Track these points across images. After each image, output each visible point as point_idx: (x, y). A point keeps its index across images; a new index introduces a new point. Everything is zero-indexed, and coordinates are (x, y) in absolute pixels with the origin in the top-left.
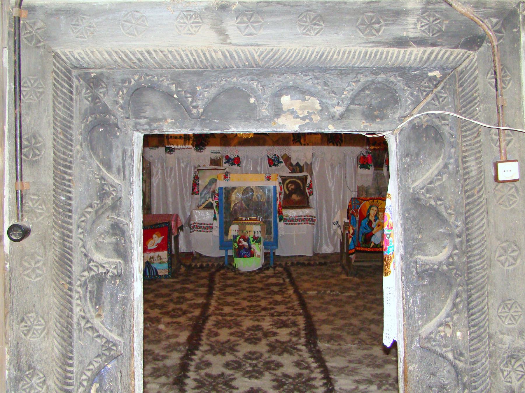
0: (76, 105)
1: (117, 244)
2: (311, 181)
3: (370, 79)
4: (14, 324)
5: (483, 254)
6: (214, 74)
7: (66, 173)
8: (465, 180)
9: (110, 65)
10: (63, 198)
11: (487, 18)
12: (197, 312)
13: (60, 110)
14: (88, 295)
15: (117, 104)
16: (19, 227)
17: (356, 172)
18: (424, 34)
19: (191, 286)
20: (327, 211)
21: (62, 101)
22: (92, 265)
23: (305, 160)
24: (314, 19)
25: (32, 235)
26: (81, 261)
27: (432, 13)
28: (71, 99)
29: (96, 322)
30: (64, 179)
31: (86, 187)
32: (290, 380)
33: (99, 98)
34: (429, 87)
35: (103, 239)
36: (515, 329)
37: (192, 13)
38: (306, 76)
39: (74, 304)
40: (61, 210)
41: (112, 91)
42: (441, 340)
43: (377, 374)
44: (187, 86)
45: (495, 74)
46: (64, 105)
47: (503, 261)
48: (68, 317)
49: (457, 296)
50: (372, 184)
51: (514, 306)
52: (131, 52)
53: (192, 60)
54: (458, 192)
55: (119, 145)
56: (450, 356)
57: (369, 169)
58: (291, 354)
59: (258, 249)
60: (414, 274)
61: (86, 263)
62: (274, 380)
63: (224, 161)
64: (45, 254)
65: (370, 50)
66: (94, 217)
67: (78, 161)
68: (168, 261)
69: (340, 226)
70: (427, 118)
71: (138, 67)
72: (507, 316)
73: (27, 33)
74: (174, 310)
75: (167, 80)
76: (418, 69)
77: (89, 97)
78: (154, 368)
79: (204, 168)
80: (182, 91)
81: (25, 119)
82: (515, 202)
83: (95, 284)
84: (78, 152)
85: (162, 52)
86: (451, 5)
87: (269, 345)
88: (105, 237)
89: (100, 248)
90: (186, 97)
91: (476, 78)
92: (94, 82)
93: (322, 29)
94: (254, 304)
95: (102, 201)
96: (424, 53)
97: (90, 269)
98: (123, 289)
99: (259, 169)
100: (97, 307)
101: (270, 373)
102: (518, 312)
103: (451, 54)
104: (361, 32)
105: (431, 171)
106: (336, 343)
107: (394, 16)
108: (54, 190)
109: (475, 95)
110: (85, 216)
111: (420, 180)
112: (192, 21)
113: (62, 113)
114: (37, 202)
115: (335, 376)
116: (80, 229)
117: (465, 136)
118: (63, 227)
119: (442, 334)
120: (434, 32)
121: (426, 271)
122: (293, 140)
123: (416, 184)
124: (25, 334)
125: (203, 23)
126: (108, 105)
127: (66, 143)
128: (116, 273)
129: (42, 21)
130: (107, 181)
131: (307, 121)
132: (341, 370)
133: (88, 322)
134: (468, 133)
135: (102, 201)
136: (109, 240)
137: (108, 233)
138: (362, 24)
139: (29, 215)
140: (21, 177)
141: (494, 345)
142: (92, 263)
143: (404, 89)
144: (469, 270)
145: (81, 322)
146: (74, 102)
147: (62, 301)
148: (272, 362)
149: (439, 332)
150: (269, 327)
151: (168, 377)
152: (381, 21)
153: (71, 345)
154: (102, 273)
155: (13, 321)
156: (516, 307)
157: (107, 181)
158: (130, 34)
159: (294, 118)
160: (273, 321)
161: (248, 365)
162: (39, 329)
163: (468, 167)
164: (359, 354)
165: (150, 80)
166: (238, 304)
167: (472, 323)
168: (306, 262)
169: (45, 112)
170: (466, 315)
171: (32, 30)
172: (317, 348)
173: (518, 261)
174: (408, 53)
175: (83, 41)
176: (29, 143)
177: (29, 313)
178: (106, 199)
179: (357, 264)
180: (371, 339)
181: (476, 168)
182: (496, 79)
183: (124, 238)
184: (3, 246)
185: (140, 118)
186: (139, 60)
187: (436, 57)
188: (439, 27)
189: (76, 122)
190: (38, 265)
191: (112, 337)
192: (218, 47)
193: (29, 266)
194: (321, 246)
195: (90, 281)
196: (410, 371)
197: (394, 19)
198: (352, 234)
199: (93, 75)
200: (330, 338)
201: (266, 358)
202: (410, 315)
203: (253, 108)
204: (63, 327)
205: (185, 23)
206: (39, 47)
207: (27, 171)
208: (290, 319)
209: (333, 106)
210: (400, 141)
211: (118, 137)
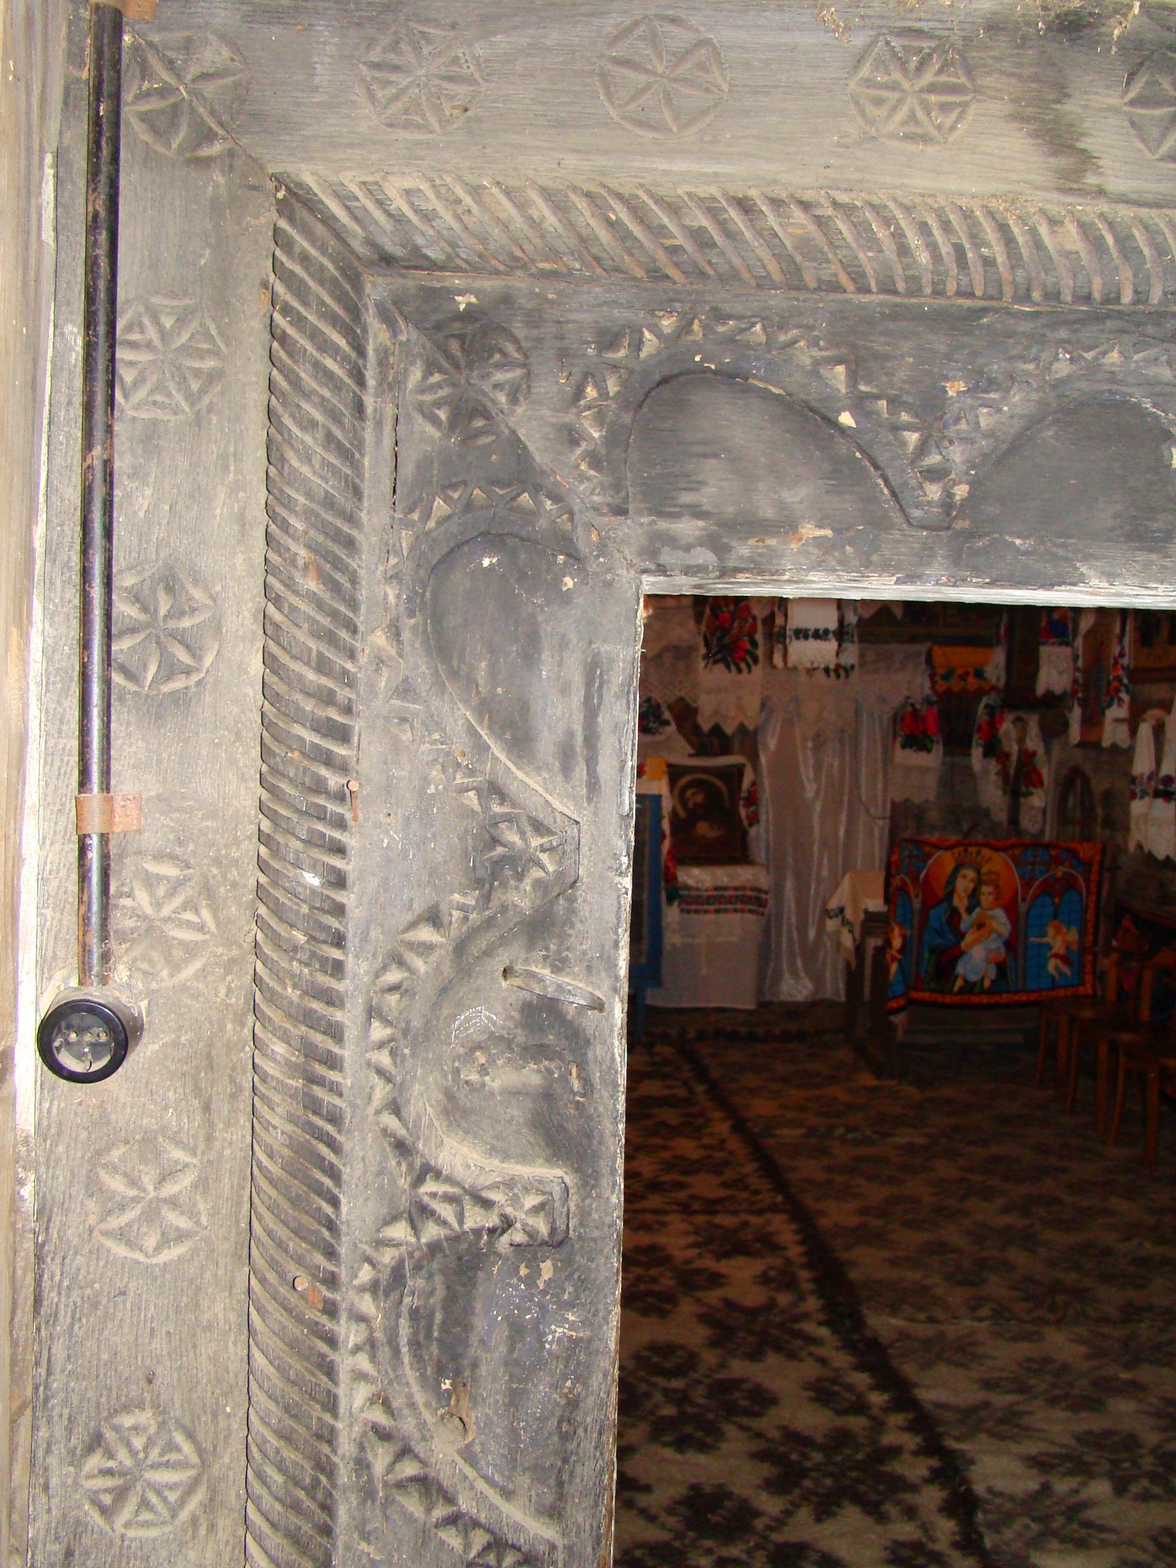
0: (378, 442)
1: (547, 1095)
2: (754, 784)
4: (52, 1461)
6: (1026, 326)
7: (328, 760)
9: (554, 254)
13: (307, 459)
14: (405, 1329)
15: (574, 442)
16: (91, 1009)
17: (887, 758)
20: (798, 876)
21: (318, 416)
22: (434, 1195)
26: (380, 1173)
28: (359, 408)
30: (319, 787)
31: (415, 826)
33: (487, 415)
35: (483, 1070)
37: (927, 45)
39: (343, 1375)
40: (300, 938)
41: (551, 384)
43: (1090, 1433)
44: (902, 374)
46: (329, 436)
48: (319, 1437)
52: (659, 201)
53: (945, 250)
55: (573, 637)
57: (929, 751)
58: (792, 1355)
61: (404, 1183)
64: (209, 1138)
66: (448, 970)
67: (378, 703)
69: (848, 923)
71: (685, 266)
73: (148, 95)
75: (814, 343)
77: (438, 404)
80: (878, 397)
81: (128, 496)
83: (438, 1279)
84: (379, 661)
85: (805, 206)
87: (705, 1318)
88: (492, 1060)
89: (466, 1113)
90: (896, 428)
92: (466, 339)
97: (420, 1213)
98: (570, 1305)
100: (447, 1385)
101: (742, 1428)
106: (922, 1316)
110: (401, 963)
112: (928, 78)
113: (311, 468)
114: (173, 892)
115: (957, 1439)
116: (376, 1024)
118: (309, 1019)
122: (706, 657)
124: (104, 1511)
125: (977, 91)
126: (531, 447)
127: (334, 614)
128: (543, 1229)
129: (223, 37)
130: (514, 805)
132: (972, 1418)
133: (405, 1452)
135: (487, 898)
136: (508, 1077)
137: (507, 1043)
139: (137, 952)
140: (106, 773)
142: (430, 1186)
145: (370, 1457)
146: (369, 424)
147: (297, 1366)
150: (692, 1253)
154: (477, 1232)
155: (48, 1451)
157: (514, 805)
158: (640, 124)
160: (696, 1233)
161: (658, 1397)
162: (172, 1487)
164: (1006, 1355)
165: (730, 340)
168: (743, 1030)
169: (226, 468)
171: (172, 81)
175: (419, 143)
176: (145, 609)
177: (126, 1408)
178: (504, 885)
180: (1025, 1299)
183: (582, 1065)
184: (11, 1102)
185: (675, 516)
186: (700, 237)
189: (374, 518)
190: (169, 1189)
191: (518, 1528)
193: (133, 1193)
194: (778, 976)
195: (418, 1267)
198: (901, 951)
199: (462, 302)
201: (710, 1369)
204: (297, 1483)
205: (893, 87)
206: (203, 163)
207: (130, 745)
208: (745, 1225)
211: (566, 599)
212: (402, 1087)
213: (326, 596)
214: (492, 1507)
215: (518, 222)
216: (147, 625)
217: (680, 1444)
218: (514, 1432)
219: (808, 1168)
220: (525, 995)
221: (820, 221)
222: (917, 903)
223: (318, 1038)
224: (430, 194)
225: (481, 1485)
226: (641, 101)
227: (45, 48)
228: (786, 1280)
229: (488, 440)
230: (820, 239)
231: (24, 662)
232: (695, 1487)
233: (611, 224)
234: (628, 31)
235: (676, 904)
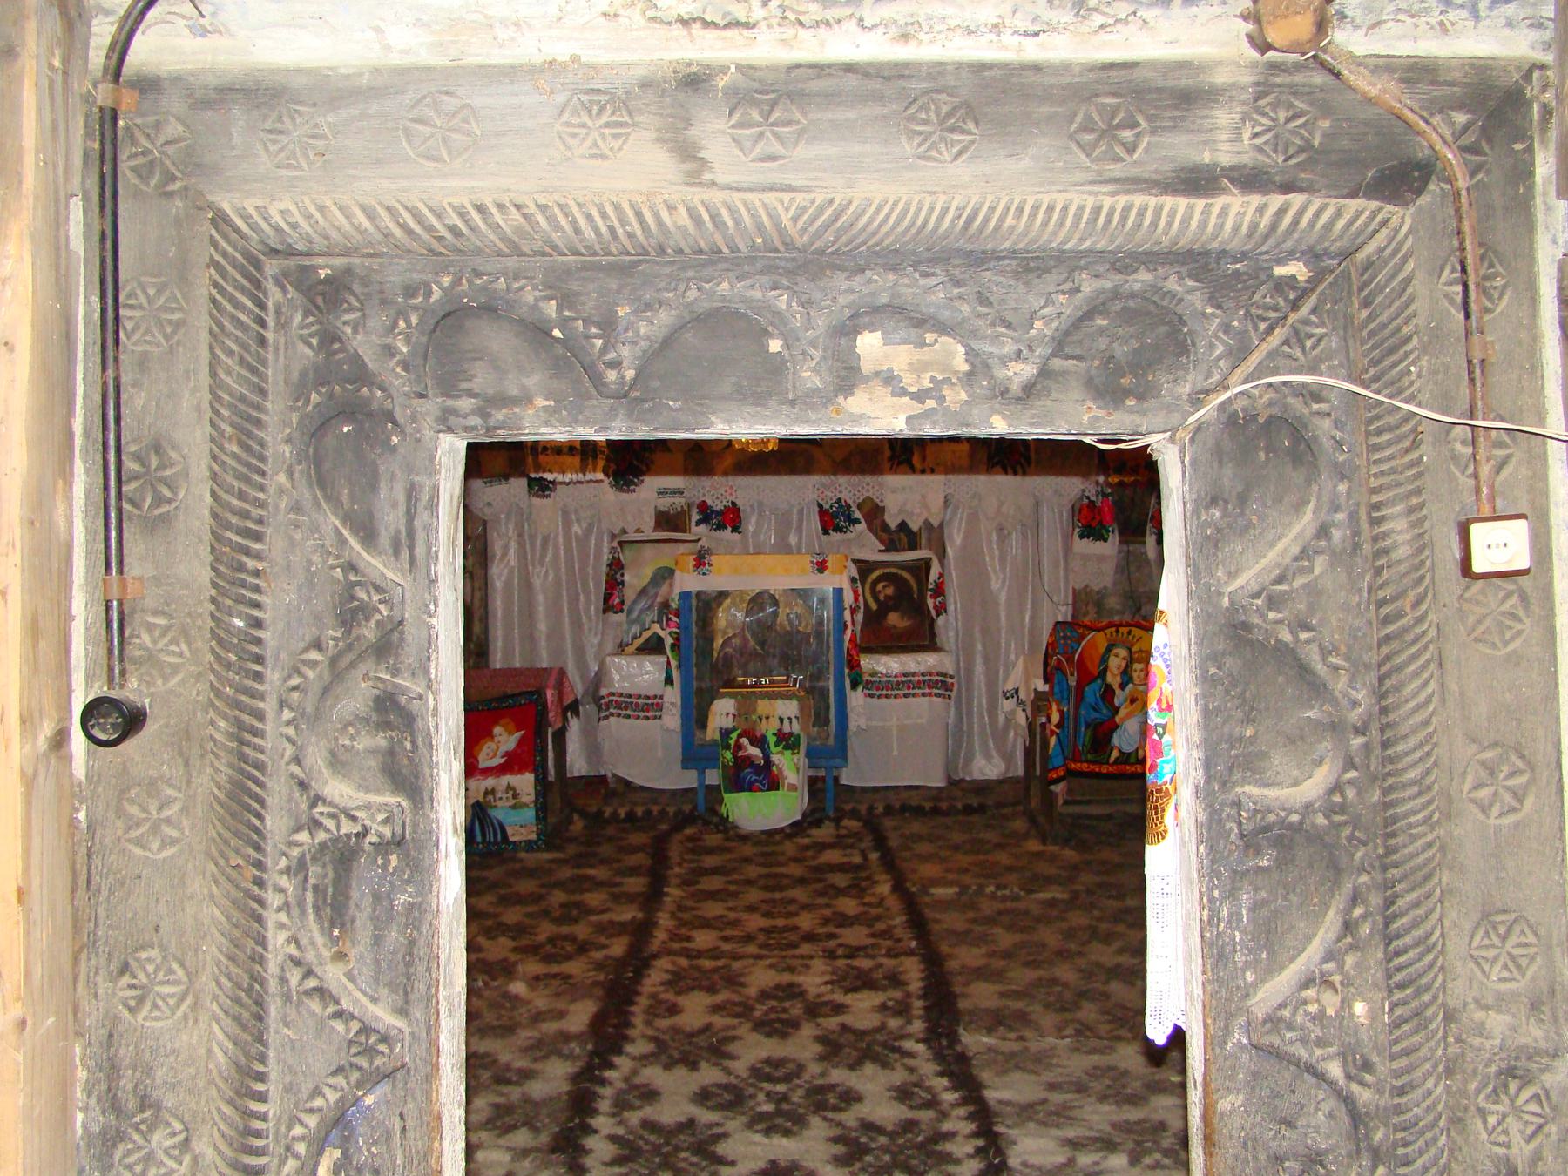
1: (391, 752)
2: (941, 575)
3: (1108, 285)
4: (99, 979)
5: (1429, 781)
6: (667, 270)
7: (247, 552)
8: (1378, 571)
10: (240, 623)
11: (1441, 112)
12: (618, 948)
13: (229, 373)
14: (309, 897)
15: (393, 355)
17: (1068, 550)
18: (1261, 158)
19: (600, 873)
20: (986, 660)
21: (235, 347)
23: (925, 515)
24: (949, 115)
25: (151, 728)
27: (1283, 98)
28: (262, 341)
29: (333, 974)
30: (242, 568)
32: (883, 1140)
33: (340, 340)
34: (1276, 309)
35: (353, 738)
36: (1520, 995)
37: (604, 98)
38: (927, 275)
39: (270, 924)
41: (378, 320)
42: (1309, 1024)
43: (1127, 1122)
44: (591, 304)
45: (1464, 270)
47: (1486, 802)
48: (253, 960)
49: (1355, 899)
50: (1115, 584)
51: (1517, 929)
53: (604, 230)
54: (1359, 605)
56: (1335, 1070)
58: (885, 1065)
59: (790, 766)
60: (1233, 837)
61: (304, 806)
62: (836, 1140)
63: (695, 517)
65: (1107, 202)
66: (327, 677)
67: (280, 517)
68: (536, 802)
70: (1270, 395)
71: (450, 249)
72: (1495, 959)
73: (136, 155)
74: (552, 940)
75: (535, 288)
76: (1243, 256)
77: (311, 335)
78: (496, 1106)
79: (638, 537)
81: (131, 398)
82: (1519, 633)
83: (329, 868)
84: (281, 491)
85: (518, 207)
86: (1338, 75)
88: (358, 732)
89: (343, 764)
90: (587, 337)
91: (1408, 281)
92: (327, 293)
93: (973, 142)
94: (780, 922)
95: (348, 632)
96: (1260, 210)
98: (409, 882)
99: (793, 540)
100: (336, 933)
101: (825, 1119)
102: (1526, 945)
103: (1338, 214)
104: (1084, 151)
105: (1280, 545)
106: (1013, 1035)
107: (1176, 107)
108: (213, 600)
109: (1406, 330)
110: (299, 673)
111: (1249, 572)
112: (605, 119)
114: (164, 634)
115: (1008, 1127)
116: (286, 711)
117: (1377, 448)
118: (239, 706)
119: (1313, 1008)
120: (1291, 151)
121: (1267, 828)
122: (891, 459)
123: (1240, 582)
124: (131, 1010)
126: (366, 359)
127: (248, 465)
128: (389, 835)
129: (178, 119)
131: (931, 403)
132: (1026, 1112)
133: (309, 973)
134: (1386, 437)
136: (368, 741)
137: (367, 720)
138: (1084, 129)
139: (143, 670)
141: (1459, 1040)
142: (320, 808)
143: (1204, 314)
144: (1390, 826)
146: (271, 349)
148: (832, 1087)
149: (1305, 1002)
150: (823, 989)
151: (536, 1130)
152: (1140, 119)
153: (260, 1039)
154: (348, 836)
155: (97, 973)
156: (1522, 932)
157: (363, 576)
158: (428, 158)
159: (894, 394)
160: (833, 973)
161: (761, 1097)
162: (172, 996)
163: (1385, 535)
164: (1077, 1064)
165: (484, 288)
166: (735, 923)
167: (1398, 977)
168: (928, 805)
169: (188, 378)
170: (1380, 955)
171: (150, 146)
172: (959, 1048)
173: (1529, 802)
174: (1215, 211)
176: (143, 465)
177: (143, 948)
178: (359, 625)
179: (1072, 809)
180: (1110, 1022)
181: (1408, 537)
182: (1465, 286)
183: (412, 735)
185: (458, 397)
186: (453, 229)
187: (1296, 222)
188: (1302, 138)
190: (166, 813)
191: (377, 1018)
192: (680, 193)
194: (969, 759)
195: (314, 859)
196: (1222, 1114)
197: (1177, 113)
198: (1057, 726)
199: (323, 273)
200: (995, 1021)
202: (1221, 956)
203: (777, 367)
204: (240, 988)
205: (584, 126)
206: (170, 195)
207: (135, 546)
209: (1004, 361)
210: (1194, 462)
211: (394, 449)
212: (301, 748)
213: (244, 455)
214: (362, 1006)
215: (347, 226)
216: (145, 474)
217: (767, 1132)
218: (377, 961)
219: (953, 920)
220: (376, 691)
221: (525, 216)
222: (1073, 681)
223: (246, 718)
224: (296, 212)
225: (359, 995)
226: (428, 143)
227: (67, 137)
228: (902, 1010)
229: (341, 356)
230: (528, 228)
231: (69, 499)
232: (773, 1162)
233: (401, 226)
234: (420, 101)
235: (860, 688)
